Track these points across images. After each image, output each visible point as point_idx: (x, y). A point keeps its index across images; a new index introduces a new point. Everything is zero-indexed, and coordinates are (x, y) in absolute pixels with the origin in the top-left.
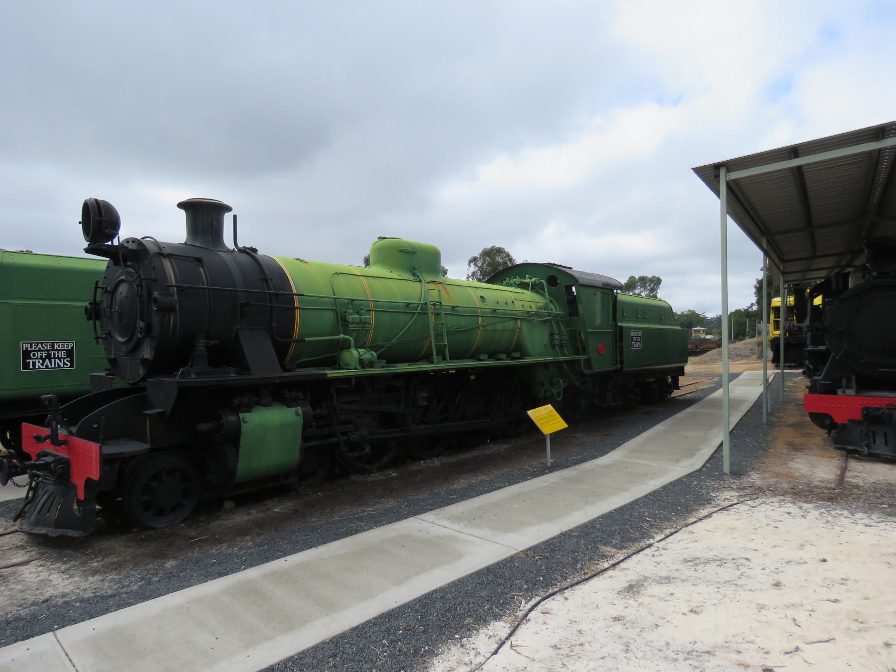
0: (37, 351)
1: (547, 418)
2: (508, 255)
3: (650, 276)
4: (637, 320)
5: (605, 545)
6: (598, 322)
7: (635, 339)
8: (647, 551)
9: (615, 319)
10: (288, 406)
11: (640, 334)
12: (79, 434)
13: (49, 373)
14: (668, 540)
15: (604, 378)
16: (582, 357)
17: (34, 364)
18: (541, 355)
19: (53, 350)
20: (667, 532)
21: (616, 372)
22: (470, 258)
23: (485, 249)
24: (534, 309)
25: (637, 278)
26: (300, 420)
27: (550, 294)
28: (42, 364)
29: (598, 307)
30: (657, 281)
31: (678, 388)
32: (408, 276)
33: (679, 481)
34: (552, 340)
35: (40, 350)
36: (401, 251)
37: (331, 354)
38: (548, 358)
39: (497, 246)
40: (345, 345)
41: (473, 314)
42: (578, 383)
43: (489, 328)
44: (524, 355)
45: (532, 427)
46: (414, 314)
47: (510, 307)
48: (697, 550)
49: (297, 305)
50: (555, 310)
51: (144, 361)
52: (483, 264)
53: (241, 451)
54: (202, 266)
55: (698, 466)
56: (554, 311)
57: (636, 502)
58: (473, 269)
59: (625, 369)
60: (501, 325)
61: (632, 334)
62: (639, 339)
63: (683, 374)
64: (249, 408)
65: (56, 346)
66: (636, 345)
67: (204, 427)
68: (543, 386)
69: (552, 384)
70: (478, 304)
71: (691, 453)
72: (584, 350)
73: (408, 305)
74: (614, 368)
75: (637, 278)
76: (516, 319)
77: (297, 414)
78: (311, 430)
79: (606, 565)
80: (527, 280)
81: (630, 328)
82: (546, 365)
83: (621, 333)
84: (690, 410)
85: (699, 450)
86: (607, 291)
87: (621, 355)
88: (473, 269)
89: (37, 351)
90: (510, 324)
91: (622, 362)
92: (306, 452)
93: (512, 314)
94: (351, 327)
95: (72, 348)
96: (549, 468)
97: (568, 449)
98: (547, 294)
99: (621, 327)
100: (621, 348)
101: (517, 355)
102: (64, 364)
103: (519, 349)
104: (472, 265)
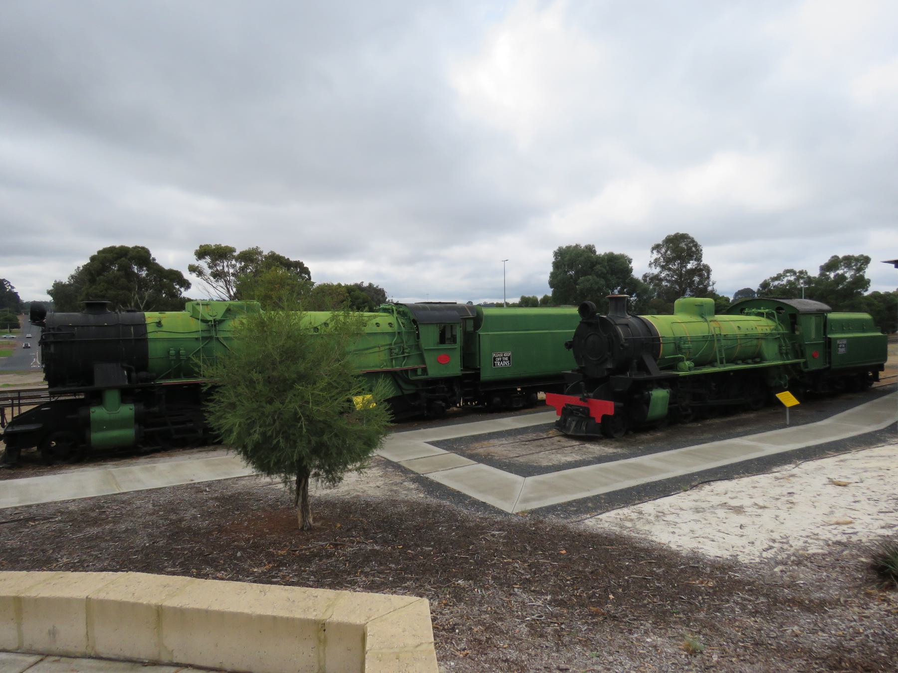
1: (788, 399)
2: (693, 241)
3: (856, 254)
4: (843, 332)
6: (813, 336)
9: (825, 333)
11: (845, 342)
12: (595, 397)
13: (502, 368)
16: (802, 360)
18: (774, 360)
22: (653, 245)
23: (669, 236)
24: (769, 331)
26: (668, 395)
27: (779, 320)
29: (813, 327)
30: (866, 260)
31: (878, 380)
32: (700, 319)
37: (673, 365)
38: (780, 362)
40: (681, 360)
41: (735, 338)
44: (763, 359)
45: (780, 404)
47: (755, 332)
48: (871, 454)
50: (782, 330)
52: (666, 251)
56: (782, 331)
58: (656, 255)
61: (838, 342)
63: (883, 370)
64: (651, 389)
66: (842, 351)
67: (636, 396)
70: (737, 332)
71: (879, 422)
72: (802, 355)
78: (673, 400)
80: (762, 311)
81: (838, 339)
82: (777, 367)
84: (887, 397)
88: (656, 255)
90: (755, 342)
91: (830, 363)
92: (670, 410)
94: (684, 351)
97: (797, 417)
100: (830, 353)
101: (758, 360)
103: (758, 356)
104: (655, 252)
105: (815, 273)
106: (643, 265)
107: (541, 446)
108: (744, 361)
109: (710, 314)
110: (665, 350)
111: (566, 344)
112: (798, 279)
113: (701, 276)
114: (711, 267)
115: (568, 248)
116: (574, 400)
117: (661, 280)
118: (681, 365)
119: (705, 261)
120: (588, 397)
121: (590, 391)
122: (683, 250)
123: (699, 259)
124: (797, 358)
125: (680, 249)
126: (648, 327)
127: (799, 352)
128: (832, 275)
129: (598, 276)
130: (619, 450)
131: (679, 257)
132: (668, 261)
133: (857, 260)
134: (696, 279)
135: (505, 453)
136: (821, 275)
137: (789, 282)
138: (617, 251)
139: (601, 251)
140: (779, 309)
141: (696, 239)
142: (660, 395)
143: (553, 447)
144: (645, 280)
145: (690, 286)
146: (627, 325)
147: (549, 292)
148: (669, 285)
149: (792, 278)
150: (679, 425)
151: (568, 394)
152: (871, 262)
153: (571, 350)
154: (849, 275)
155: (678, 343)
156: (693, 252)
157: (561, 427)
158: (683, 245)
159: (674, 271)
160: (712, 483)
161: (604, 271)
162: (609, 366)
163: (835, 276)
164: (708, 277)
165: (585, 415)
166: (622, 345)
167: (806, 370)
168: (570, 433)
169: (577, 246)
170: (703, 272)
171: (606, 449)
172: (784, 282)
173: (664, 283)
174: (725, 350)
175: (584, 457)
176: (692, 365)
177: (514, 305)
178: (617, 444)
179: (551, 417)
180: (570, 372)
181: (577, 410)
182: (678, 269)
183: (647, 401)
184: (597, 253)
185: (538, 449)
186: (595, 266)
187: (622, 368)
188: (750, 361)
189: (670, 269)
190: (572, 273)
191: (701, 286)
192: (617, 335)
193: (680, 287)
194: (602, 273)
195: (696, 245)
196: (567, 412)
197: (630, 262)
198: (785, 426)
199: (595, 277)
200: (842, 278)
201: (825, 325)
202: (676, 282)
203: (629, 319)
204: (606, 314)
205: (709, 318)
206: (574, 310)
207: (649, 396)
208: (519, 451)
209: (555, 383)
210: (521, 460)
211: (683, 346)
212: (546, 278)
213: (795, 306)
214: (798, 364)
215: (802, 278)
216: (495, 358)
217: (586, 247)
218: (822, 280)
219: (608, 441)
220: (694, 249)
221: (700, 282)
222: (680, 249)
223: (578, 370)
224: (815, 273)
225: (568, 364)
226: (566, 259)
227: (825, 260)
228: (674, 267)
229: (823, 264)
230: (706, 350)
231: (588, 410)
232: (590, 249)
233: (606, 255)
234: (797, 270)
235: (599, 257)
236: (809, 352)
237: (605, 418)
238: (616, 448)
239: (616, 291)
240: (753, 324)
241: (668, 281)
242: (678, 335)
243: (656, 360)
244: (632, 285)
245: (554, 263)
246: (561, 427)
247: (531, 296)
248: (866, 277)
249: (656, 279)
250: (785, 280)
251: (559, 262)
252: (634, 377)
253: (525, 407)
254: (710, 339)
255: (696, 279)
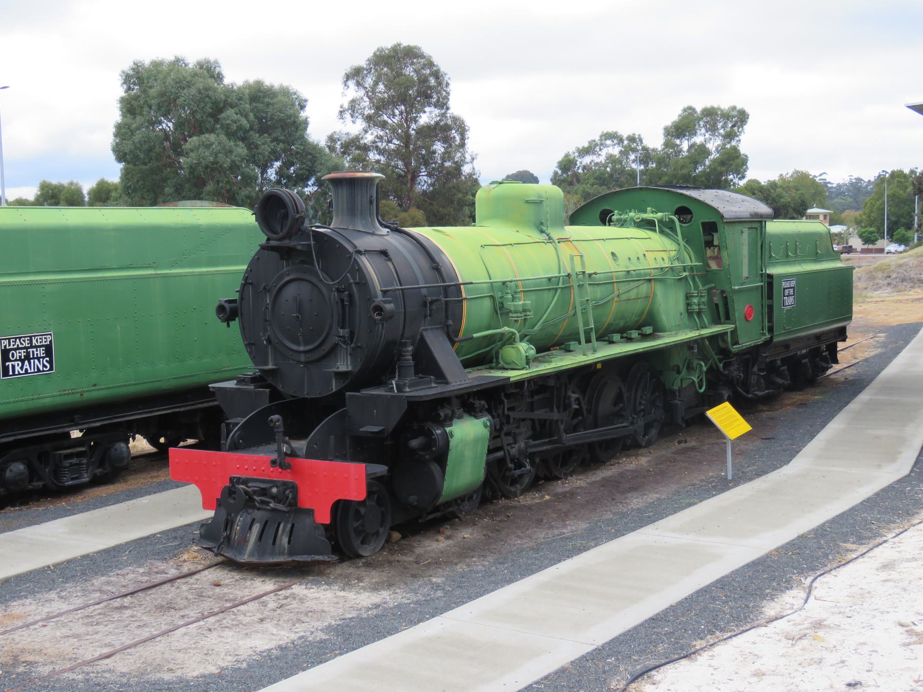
0: (15, 350)
1: (727, 419)
2: (431, 64)
3: (725, 105)
5: (845, 542)
6: (745, 273)
7: (787, 292)
8: (884, 545)
10: (476, 417)
12: (310, 454)
14: (900, 536)
15: (753, 353)
16: (728, 327)
17: (13, 367)
18: (680, 328)
19: (32, 347)
20: (897, 531)
21: (768, 343)
22: (347, 68)
23: (381, 50)
24: (667, 264)
25: (699, 109)
26: (486, 432)
28: (22, 368)
29: (745, 251)
30: (742, 118)
32: (529, 235)
33: (890, 488)
34: (688, 305)
35: (18, 348)
36: (527, 202)
37: (485, 355)
39: (405, 43)
40: (509, 340)
41: (609, 282)
42: (721, 365)
43: (624, 297)
46: (556, 289)
49: (464, 295)
50: (690, 260)
51: (340, 375)
52: (376, 83)
53: (448, 468)
54: (390, 260)
55: (906, 471)
57: (853, 510)
58: (353, 92)
59: (776, 340)
60: (635, 291)
62: (791, 291)
64: (449, 420)
65: (34, 341)
67: (415, 443)
68: (679, 372)
69: (690, 368)
70: (612, 267)
71: (892, 456)
73: (549, 279)
74: (763, 338)
75: (699, 109)
76: (650, 280)
77: (486, 426)
79: (854, 556)
80: (649, 216)
82: (688, 345)
83: (770, 285)
84: (864, 397)
85: (900, 453)
86: (754, 225)
87: (770, 320)
89: (15, 350)
91: (771, 330)
93: (646, 275)
95: (51, 342)
96: (730, 481)
98: (680, 238)
99: (770, 276)
100: (771, 308)
101: (648, 330)
102: (44, 366)
103: (647, 323)
104: (351, 83)
105: (655, 141)
106: (329, 115)
107: (169, 607)
108: (605, 336)
109: (560, 224)
110: (474, 316)
111: (221, 309)
112: (625, 153)
113: (447, 140)
114: (468, 122)
115: (156, 65)
116: (255, 463)
117: (366, 148)
118: (509, 352)
119: (458, 106)
120: (293, 454)
121: (300, 435)
122: (409, 83)
123: (442, 104)
124: (716, 321)
125: (403, 80)
126: (431, 257)
127: (721, 310)
128: (685, 145)
129: (230, 135)
130: (385, 596)
131: (403, 99)
132: (381, 106)
133: (726, 116)
134: (439, 147)
135: (66, 646)
136: (667, 144)
137: (610, 157)
138: (273, 79)
139: (235, 77)
140: (683, 212)
141: (436, 60)
142: (468, 433)
143: (207, 605)
144: (332, 149)
145: (426, 164)
146: (384, 253)
147: (114, 172)
148: (383, 159)
149: (616, 151)
150: (503, 502)
151: (235, 447)
152: (750, 121)
153: (235, 324)
154: (714, 145)
155: (500, 299)
156: (430, 88)
157: (216, 540)
158: (409, 71)
159: (394, 130)
160: (657, 675)
161: (244, 122)
162: (344, 365)
163: (691, 147)
164: (462, 145)
165: (287, 503)
166: (379, 309)
167: (735, 349)
168: (245, 558)
169: (177, 60)
170: (449, 131)
171: (351, 595)
172: (601, 158)
173: (373, 156)
174: (596, 307)
175: (301, 630)
176: (533, 352)
177: (21, 203)
178: (375, 576)
179: (179, 506)
180: (231, 384)
181: (264, 492)
182: (400, 126)
183: (441, 455)
184: (227, 81)
185: (163, 622)
186: (221, 111)
187: (378, 369)
188: (635, 334)
189: (383, 125)
190: (168, 125)
191: (448, 164)
192: (363, 283)
193: (407, 164)
194: (240, 128)
195: (437, 75)
196: (232, 500)
197: (302, 107)
198: (724, 485)
199: (223, 138)
200: (701, 152)
201: (763, 248)
202: (397, 153)
203: (385, 238)
204: (326, 223)
205: (556, 234)
206: (244, 217)
207: (447, 438)
208: (111, 634)
209: (183, 418)
210: (122, 665)
211: (510, 305)
212: (106, 139)
213: (714, 204)
214: (723, 335)
215: (634, 150)
216: (6, 352)
217: (201, 65)
218: (668, 156)
219: (345, 568)
220: (432, 81)
221: (447, 155)
222: (403, 80)
223: (254, 380)
224: (655, 141)
225: (223, 359)
226: (152, 92)
227: (672, 116)
228: (394, 119)
229: (669, 123)
230: (557, 315)
231: (294, 488)
232: (209, 71)
233: (248, 86)
234: (625, 133)
235: (229, 91)
236: (739, 307)
237: (341, 508)
238: (375, 588)
239: (272, 174)
240: (630, 249)
241: (381, 152)
242: (498, 277)
243: (453, 343)
244: (306, 160)
245: (122, 100)
246: (216, 540)
247: (65, 182)
248: (743, 149)
249: (352, 145)
250: (604, 152)
251: (136, 98)
252: (409, 392)
253: (96, 482)
254: (561, 285)
255: (439, 147)
